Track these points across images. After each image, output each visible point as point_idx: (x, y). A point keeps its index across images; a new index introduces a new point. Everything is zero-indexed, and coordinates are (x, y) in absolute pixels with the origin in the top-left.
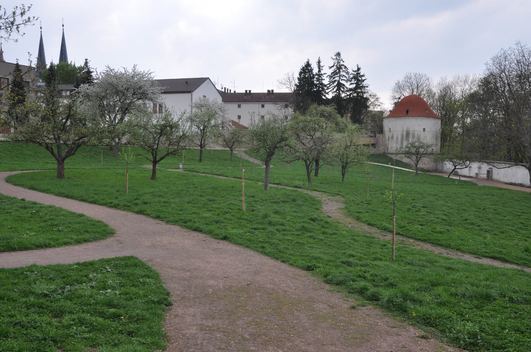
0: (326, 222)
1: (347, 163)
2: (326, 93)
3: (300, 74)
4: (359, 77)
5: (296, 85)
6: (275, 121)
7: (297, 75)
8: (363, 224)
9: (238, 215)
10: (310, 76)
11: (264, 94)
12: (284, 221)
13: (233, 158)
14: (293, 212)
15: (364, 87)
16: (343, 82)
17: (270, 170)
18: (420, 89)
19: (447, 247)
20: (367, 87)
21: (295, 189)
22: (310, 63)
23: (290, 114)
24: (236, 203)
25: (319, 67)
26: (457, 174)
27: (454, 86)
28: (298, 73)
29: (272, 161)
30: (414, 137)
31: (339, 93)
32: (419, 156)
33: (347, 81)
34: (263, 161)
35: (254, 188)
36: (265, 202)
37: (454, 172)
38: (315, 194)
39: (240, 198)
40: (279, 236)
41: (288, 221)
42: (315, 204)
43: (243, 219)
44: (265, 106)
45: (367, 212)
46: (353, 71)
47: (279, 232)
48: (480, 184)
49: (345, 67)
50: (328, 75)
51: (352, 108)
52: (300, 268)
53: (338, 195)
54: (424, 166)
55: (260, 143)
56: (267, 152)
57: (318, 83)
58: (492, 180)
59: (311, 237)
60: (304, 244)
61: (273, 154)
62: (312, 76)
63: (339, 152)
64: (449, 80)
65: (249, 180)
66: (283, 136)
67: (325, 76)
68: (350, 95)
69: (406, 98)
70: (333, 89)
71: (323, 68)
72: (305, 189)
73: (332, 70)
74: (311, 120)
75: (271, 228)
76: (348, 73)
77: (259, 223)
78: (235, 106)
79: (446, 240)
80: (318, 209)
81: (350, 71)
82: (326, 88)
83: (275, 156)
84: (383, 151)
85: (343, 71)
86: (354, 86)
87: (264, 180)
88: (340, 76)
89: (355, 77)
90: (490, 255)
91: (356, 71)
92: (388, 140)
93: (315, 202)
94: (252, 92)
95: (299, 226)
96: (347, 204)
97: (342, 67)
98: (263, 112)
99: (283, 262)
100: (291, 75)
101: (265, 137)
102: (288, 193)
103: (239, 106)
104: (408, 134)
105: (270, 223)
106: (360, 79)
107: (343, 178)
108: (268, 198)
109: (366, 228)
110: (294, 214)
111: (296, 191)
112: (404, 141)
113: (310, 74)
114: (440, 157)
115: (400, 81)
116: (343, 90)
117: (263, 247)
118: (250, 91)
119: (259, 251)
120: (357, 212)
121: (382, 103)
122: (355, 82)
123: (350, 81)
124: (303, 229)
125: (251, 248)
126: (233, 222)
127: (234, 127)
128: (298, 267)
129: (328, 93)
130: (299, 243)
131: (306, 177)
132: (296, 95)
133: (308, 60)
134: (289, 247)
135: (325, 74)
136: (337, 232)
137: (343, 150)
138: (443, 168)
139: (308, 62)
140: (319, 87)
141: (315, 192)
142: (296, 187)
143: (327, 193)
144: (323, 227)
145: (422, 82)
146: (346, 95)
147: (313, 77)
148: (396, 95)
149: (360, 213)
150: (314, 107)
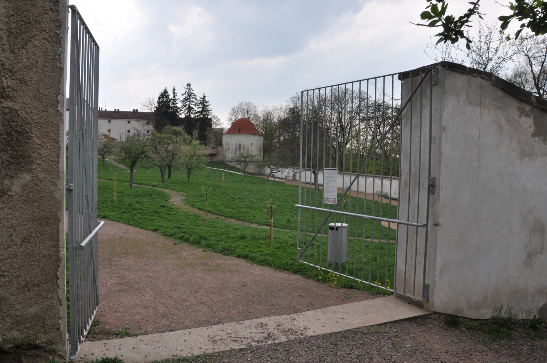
0: (171, 208)
1: (191, 169)
2: (179, 114)
3: (159, 98)
4: (205, 102)
5: (156, 107)
6: (139, 135)
7: (156, 99)
8: (195, 209)
9: (112, 205)
10: (167, 101)
11: (130, 112)
12: (143, 207)
13: (105, 164)
14: (150, 202)
15: (209, 110)
16: (192, 106)
17: (134, 174)
18: (249, 114)
19: (243, 220)
20: (211, 110)
21: (152, 187)
22: (167, 90)
23: (151, 129)
24: (110, 197)
25: (174, 93)
26: (273, 176)
27: (273, 113)
28: (158, 98)
29: (136, 167)
30: (244, 149)
31: (189, 114)
32: (247, 163)
33: (195, 105)
34: (129, 167)
35: (122, 187)
36: (130, 196)
37: (271, 175)
38: (166, 191)
39: (112, 194)
40: (138, 215)
41: (146, 207)
42: (165, 197)
43: (115, 207)
44: (131, 122)
45: (199, 202)
46: (200, 98)
47: (139, 214)
48: (287, 183)
49: (194, 95)
50: (181, 100)
51: (199, 126)
52: (150, 230)
53: (183, 191)
55: (126, 154)
56: (131, 161)
57: (173, 106)
58: (296, 180)
59: (159, 216)
60: (154, 220)
61: (136, 162)
62: (168, 100)
63: (185, 161)
64: (270, 108)
65: (118, 181)
66: (143, 150)
67: (179, 101)
68: (198, 116)
69: (239, 120)
70: (185, 111)
71: (177, 95)
72: (160, 187)
73: (184, 97)
74: (165, 137)
75: (134, 212)
76: (196, 99)
77: (126, 209)
78: (106, 121)
79: (244, 217)
80: (167, 200)
81: (198, 98)
82: (179, 110)
83: (137, 164)
84: (222, 159)
85: (193, 98)
86: (201, 109)
87: (130, 181)
88: (190, 102)
89: (201, 102)
90: (267, 224)
91: (202, 98)
92: (226, 151)
93: (165, 196)
94: (120, 110)
95: (152, 210)
96: (187, 197)
97: (192, 94)
98: (129, 127)
99: (141, 228)
100: (151, 99)
101: (130, 150)
102: (146, 190)
103: (109, 122)
104: (240, 147)
105: (133, 209)
106: (206, 104)
107: (189, 179)
108: (133, 193)
109: (196, 211)
110: (150, 203)
111: (153, 188)
112: (237, 152)
113: (167, 99)
114: (261, 165)
115: (235, 107)
116: (192, 112)
117: (129, 222)
118: (118, 110)
119: (126, 224)
120: (192, 202)
121: (222, 123)
122: (202, 106)
123: (198, 106)
124: (156, 212)
125: (121, 222)
126: (108, 209)
127: (105, 139)
128: (149, 230)
129: (180, 114)
130: (152, 219)
131: (161, 179)
132: (156, 115)
133: (166, 88)
134: (145, 222)
135: (178, 99)
136: (177, 213)
137: (189, 160)
138: (265, 172)
139: (165, 90)
140: (174, 109)
141: (166, 189)
142: (153, 186)
143: (175, 190)
144: (168, 211)
145: (250, 109)
146: (195, 116)
147: (170, 102)
148: (232, 117)
149: (194, 202)
150: (169, 128)
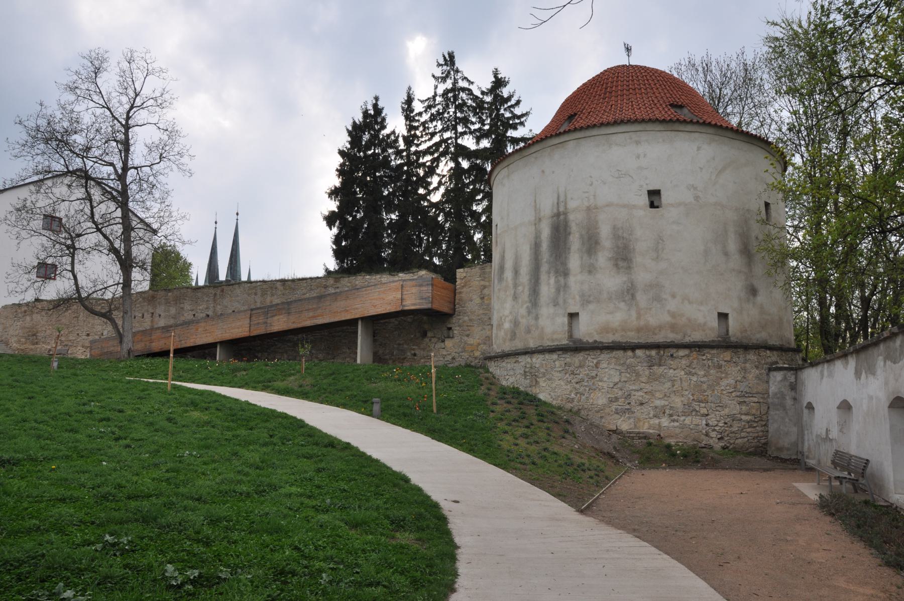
54: (665, 422)
112: (543, 277)
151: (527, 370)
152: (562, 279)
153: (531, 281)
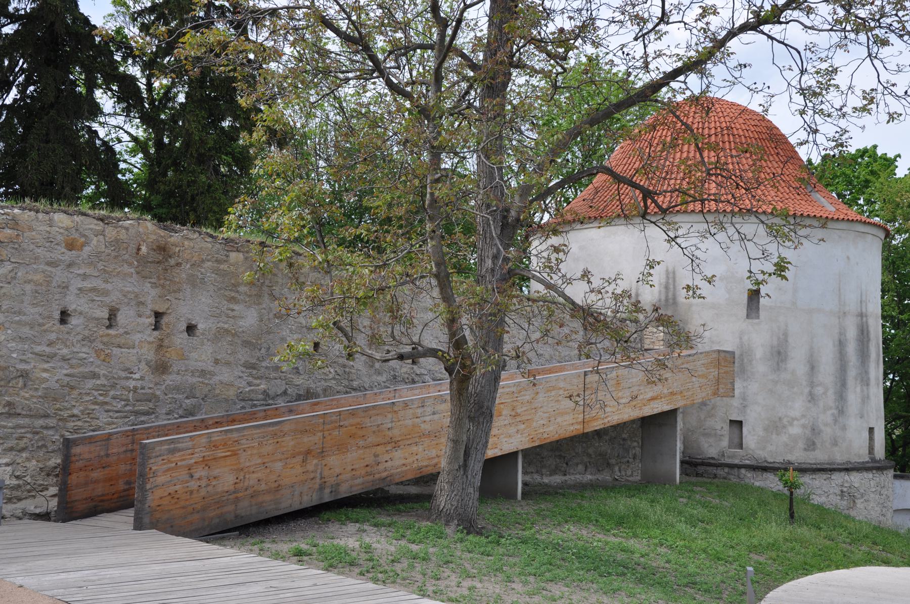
151: (845, 489)
152: (865, 388)
153: (836, 384)
